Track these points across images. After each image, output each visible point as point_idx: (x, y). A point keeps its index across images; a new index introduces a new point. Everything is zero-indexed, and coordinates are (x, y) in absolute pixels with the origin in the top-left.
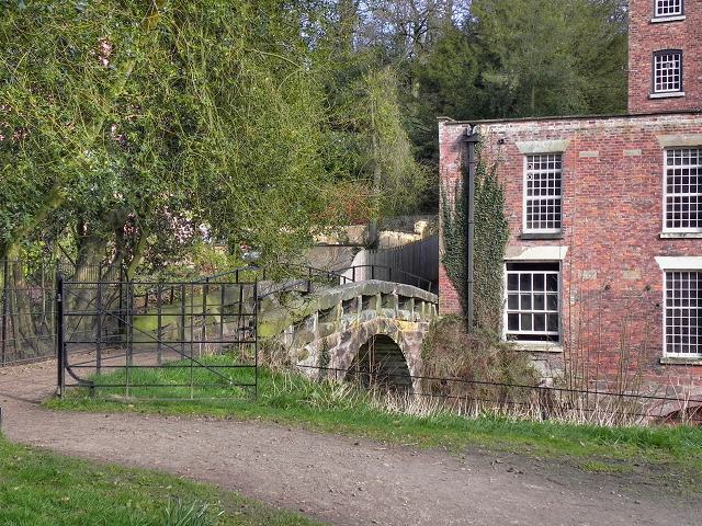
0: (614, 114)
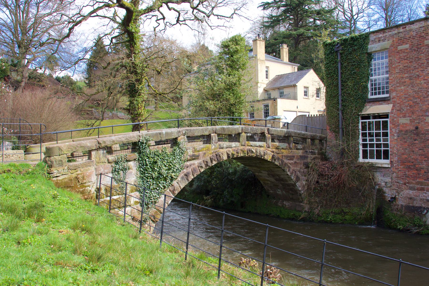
0: (288, 75)
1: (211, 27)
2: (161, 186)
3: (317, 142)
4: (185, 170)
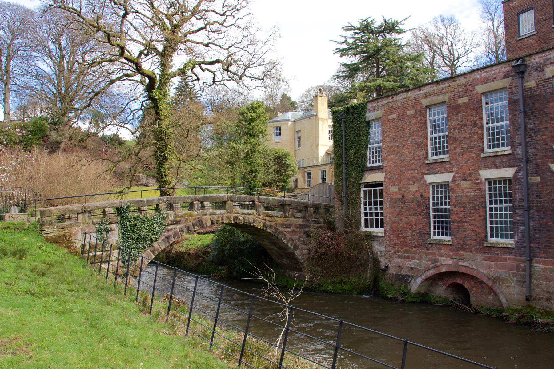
1: (248, 87)
2: (141, 246)
3: (322, 211)
4: (166, 233)
